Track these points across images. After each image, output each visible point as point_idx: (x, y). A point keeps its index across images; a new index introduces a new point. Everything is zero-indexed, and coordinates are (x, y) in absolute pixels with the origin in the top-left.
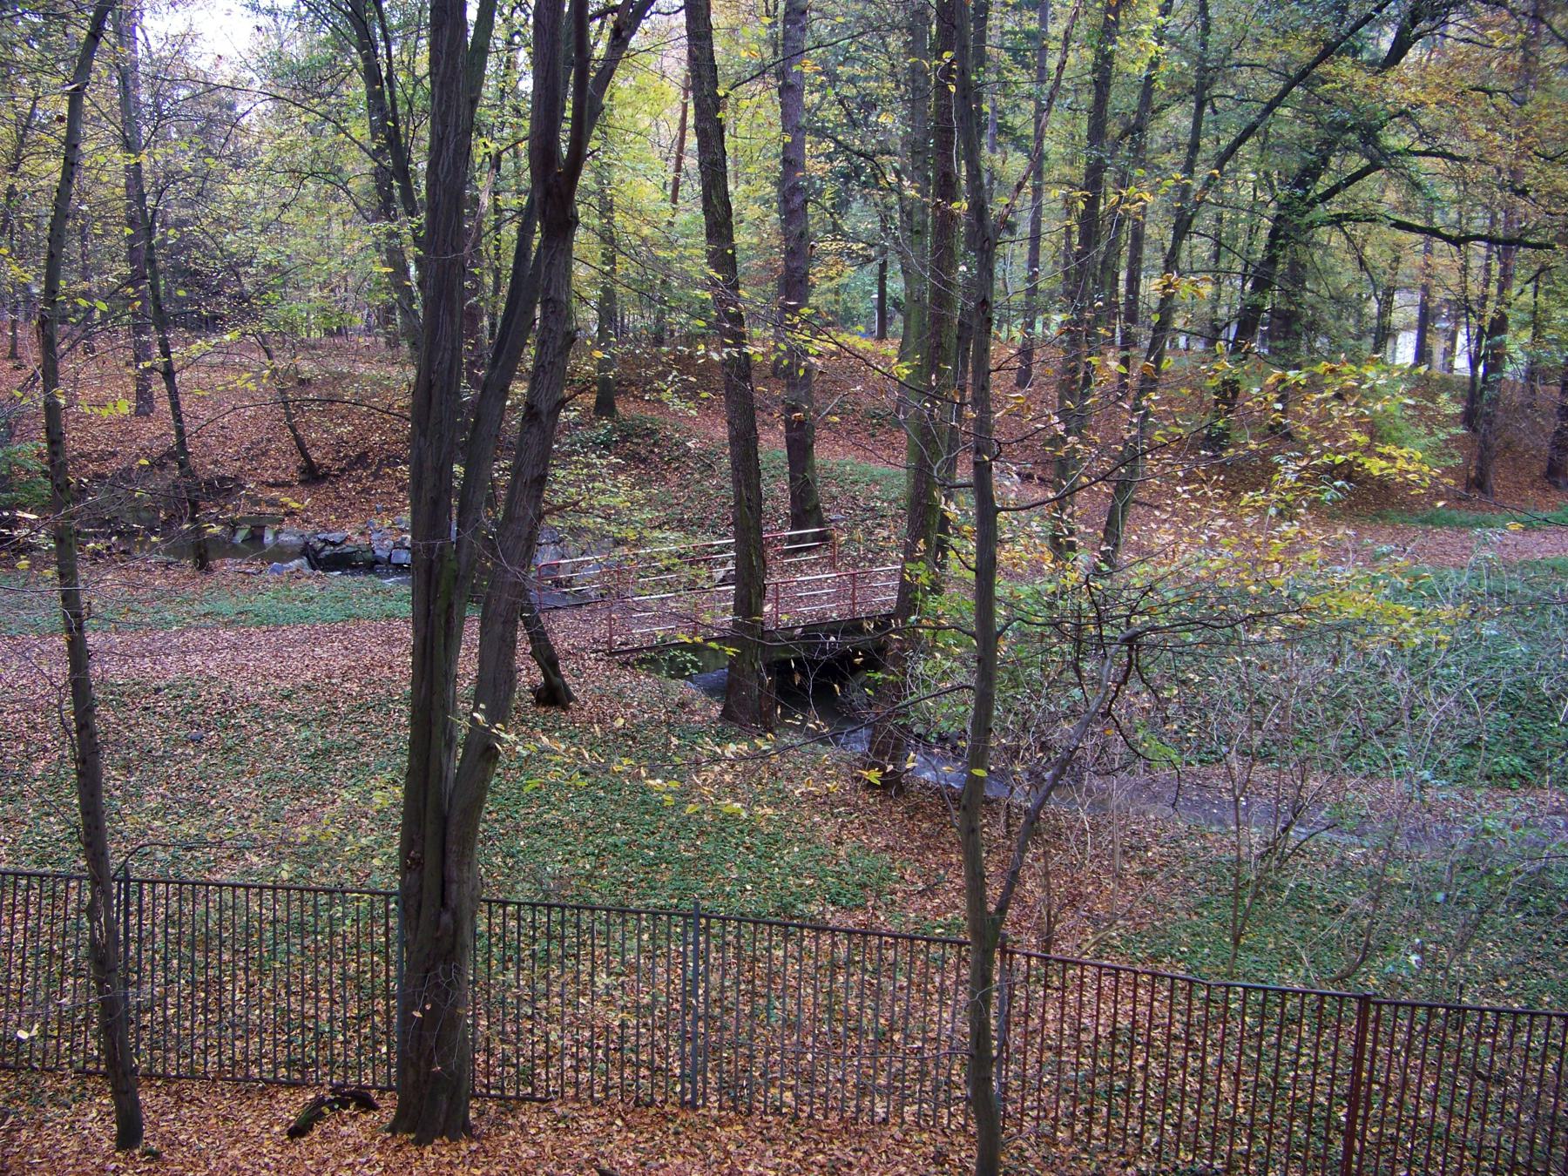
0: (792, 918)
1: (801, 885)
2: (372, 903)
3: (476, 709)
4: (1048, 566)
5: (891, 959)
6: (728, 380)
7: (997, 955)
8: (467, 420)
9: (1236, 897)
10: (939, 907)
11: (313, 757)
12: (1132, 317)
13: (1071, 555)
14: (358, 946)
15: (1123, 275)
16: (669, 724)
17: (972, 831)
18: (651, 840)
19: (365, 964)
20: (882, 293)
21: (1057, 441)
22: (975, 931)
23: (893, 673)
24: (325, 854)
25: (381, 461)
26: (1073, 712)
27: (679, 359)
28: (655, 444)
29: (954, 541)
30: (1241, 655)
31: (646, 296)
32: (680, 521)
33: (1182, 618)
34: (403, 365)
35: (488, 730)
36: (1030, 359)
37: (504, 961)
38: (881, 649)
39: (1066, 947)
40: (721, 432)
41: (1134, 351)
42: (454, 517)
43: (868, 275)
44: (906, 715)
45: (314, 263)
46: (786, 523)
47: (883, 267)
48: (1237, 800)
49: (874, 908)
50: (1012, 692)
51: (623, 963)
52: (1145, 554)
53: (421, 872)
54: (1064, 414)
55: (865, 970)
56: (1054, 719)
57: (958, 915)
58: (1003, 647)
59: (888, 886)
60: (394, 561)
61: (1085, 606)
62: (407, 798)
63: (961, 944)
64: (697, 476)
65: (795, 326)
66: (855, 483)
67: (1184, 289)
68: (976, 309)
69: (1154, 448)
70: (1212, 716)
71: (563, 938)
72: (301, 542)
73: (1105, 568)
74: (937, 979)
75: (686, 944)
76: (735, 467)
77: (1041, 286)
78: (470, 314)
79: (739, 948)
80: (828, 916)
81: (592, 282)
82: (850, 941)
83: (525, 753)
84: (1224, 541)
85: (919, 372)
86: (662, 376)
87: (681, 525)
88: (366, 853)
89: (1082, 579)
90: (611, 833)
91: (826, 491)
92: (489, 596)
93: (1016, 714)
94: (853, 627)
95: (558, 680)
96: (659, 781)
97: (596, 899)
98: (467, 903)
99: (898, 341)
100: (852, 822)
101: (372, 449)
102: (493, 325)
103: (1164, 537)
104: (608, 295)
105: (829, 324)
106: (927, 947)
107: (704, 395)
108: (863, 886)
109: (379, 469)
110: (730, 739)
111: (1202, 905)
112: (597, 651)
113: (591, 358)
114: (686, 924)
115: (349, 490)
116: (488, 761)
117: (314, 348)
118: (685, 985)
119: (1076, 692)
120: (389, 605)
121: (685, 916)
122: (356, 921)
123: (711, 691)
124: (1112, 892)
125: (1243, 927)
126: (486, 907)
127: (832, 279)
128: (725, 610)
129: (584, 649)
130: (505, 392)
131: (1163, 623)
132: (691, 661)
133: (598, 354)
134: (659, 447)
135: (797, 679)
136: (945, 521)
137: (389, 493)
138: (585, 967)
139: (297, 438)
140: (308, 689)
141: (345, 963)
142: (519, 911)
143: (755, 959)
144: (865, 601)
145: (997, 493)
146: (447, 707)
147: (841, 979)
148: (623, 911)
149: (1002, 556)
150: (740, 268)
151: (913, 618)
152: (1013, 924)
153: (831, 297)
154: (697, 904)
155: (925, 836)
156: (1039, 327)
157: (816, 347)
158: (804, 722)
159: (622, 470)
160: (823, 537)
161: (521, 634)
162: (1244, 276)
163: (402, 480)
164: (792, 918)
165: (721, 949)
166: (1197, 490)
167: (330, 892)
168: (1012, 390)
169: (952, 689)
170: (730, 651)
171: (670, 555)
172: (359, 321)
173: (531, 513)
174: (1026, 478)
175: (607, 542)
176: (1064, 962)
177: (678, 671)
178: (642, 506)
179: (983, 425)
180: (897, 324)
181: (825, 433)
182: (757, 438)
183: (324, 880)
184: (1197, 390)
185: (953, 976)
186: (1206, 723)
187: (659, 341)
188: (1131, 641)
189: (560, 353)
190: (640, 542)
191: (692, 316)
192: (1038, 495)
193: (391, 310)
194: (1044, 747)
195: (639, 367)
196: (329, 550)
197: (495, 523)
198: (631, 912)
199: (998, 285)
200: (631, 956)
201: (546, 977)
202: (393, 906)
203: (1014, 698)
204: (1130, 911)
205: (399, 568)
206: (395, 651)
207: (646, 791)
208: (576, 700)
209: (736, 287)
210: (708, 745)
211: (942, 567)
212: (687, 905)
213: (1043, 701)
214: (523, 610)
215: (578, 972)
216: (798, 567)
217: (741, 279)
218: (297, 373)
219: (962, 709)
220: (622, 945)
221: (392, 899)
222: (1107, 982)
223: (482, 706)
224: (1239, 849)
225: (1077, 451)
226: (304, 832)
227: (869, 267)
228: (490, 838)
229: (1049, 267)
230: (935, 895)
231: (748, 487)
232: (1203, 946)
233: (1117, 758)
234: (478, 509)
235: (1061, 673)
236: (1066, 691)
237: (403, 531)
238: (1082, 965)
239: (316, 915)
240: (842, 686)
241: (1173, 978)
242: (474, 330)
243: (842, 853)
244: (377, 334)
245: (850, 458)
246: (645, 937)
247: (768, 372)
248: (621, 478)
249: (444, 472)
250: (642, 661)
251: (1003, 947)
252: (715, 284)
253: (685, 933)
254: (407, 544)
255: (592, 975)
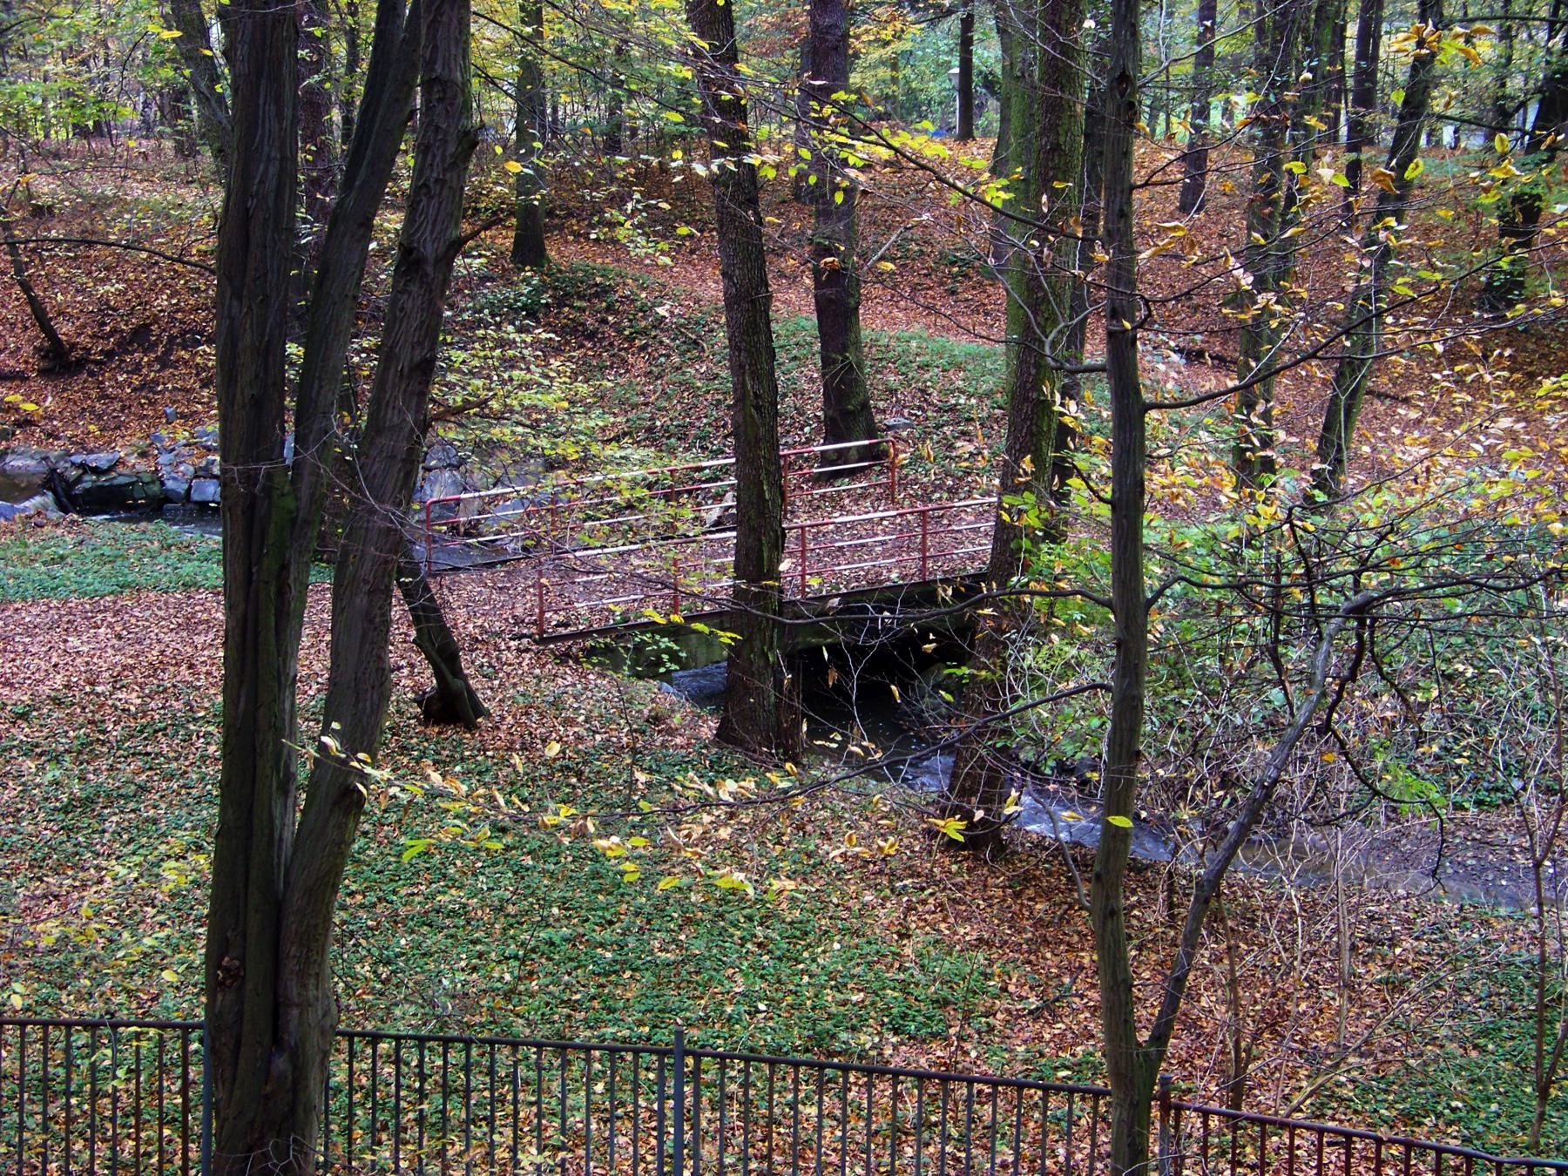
0: (831, 1054)
1: (844, 1003)
2: (161, 1043)
3: (326, 730)
4: (1227, 495)
5: (987, 1119)
6: (722, 209)
7: (1155, 1113)
8: (309, 272)
9: (1541, 1022)
10: (1063, 1035)
11: (66, 810)
12: (1365, 97)
13: (1267, 479)
14: (137, 1113)
15: (1352, 30)
16: (634, 751)
17: (1109, 913)
18: (607, 935)
19: (149, 1142)
20: (966, 64)
21: (1240, 299)
22: (1117, 1074)
23: (987, 668)
24: (85, 964)
25: (171, 339)
26: (1271, 724)
27: (643, 176)
28: (610, 309)
29: (1081, 461)
30: (1542, 632)
31: (591, 75)
32: (650, 430)
33: (1444, 575)
34: (204, 186)
35: (345, 762)
36: (1199, 167)
37: (374, 1130)
38: (968, 628)
39: (1266, 1100)
40: (713, 289)
41: (1366, 154)
42: (290, 427)
43: (945, 36)
44: (1007, 733)
45: (51, 17)
46: (817, 431)
47: (968, 24)
48: (1538, 865)
49: (960, 1038)
50: (1174, 694)
51: (563, 1130)
52: (1381, 475)
53: (240, 989)
54: (1251, 258)
55: (946, 1138)
56: (1242, 738)
57: (1093, 1049)
58: (1157, 627)
59: (982, 1003)
60: (195, 497)
61: (1288, 556)
62: (217, 873)
63: (1098, 1094)
64: (676, 359)
65: (825, 121)
66: (924, 367)
67: (1450, 50)
68: (1111, 89)
69: (1398, 305)
70: (1495, 731)
71: (467, 1091)
72: (43, 468)
73: (1321, 497)
74: (1061, 1151)
75: (662, 1099)
76: (734, 345)
77: (1220, 49)
78: (311, 103)
79: (747, 1103)
80: (888, 1051)
81: (505, 52)
82: (920, 1088)
83: (404, 797)
84: (1511, 453)
85: (1026, 192)
86: (618, 201)
87: (652, 437)
88: (152, 962)
89: (1282, 516)
90: (545, 923)
91: (878, 381)
92: (345, 553)
93: (1181, 730)
94: (922, 593)
95: (459, 683)
96: (615, 839)
97: (520, 1028)
98: (315, 1038)
99: (991, 142)
100: (924, 902)
101: (156, 319)
102: (347, 120)
103: (1412, 450)
104: (530, 72)
105: (879, 117)
106: (1045, 1099)
107: (683, 230)
108: (943, 1003)
109: (168, 352)
110: (731, 773)
111: (1485, 1033)
112: (520, 637)
113: (506, 173)
114: (662, 1066)
115: (120, 386)
116: (347, 813)
117: (57, 156)
118: (661, 1164)
119: (1276, 695)
120: (188, 568)
121: (662, 1054)
122: (134, 1072)
123: (701, 698)
124: (1339, 1012)
125: (1553, 1070)
126: (345, 1045)
127: (887, 43)
128: (721, 569)
129: (499, 634)
130: (366, 228)
131: (1413, 582)
132: (668, 650)
133: (514, 167)
134: (616, 313)
135: (833, 676)
136: (1065, 431)
137: (184, 390)
138: (504, 1137)
139: (32, 301)
140: (57, 702)
141: (115, 1141)
142: (397, 1050)
143: (772, 1121)
144: (942, 554)
145: (1144, 380)
146: (281, 725)
147: (909, 1151)
148: (563, 1047)
149: (1155, 482)
150: (741, 28)
151: (1015, 579)
152: (1181, 1063)
153: (884, 73)
154: (680, 1035)
155: (1039, 923)
156: (1216, 117)
157: (861, 152)
158: (843, 745)
159: (558, 351)
160: (874, 454)
161: (398, 610)
162: (1552, 24)
163: (205, 368)
164: (831, 1054)
165: (718, 1106)
166: (1468, 373)
167: (92, 1026)
168: (1172, 217)
169: (1079, 690)
170: (726, 637)
171: (634, 483)
172: (129, 114)
173: (410, 418)
174: (1193, 356)
175: (533, 465)
176: (1262, 1122)
177: (648, 667)
178: (589, 407)
179: (1122, 273)
180: (990, 115)
181: (877, 290)
182: (769, 298)
183: (83, 1007)
184: (1473, 213)
185: (1086, 1145)
186: (1485, 740)
187: (613, 146)
188: (1362, 612)
189: (453, 165)
190: (586, 463)
191: (664, 105)
192: (1210, 384)
193: (180, 95)
194: (1226, 782)
195: (583, 186)
196: (89, 481)
197: (355, 434)
198: (576, 1047)
199: (1148, 50)
200: (576, 1119)
201: (441, 1153)
202: (195, 1046)
203: (1177, 703)
204: (1366, 1042)
205: (201, 512)
206: (199, 640)
207: (597, 857)
208: (488, 715)
209: (732, 57)
210: (694, 783)
211: (1061, 497)
212: (664, 1037)
213: (1223, 709)
214: (401, 573)
215: (492, 1144)
216: (836, 502)
217: (741, 46)
218: (30, 197)
219: (1095, 722)
220: (562, 1102)
221: (194, 1035)
222: (1332, 1155)
223: (335, 726)
224: (1543, 944)
225: (1273, 315)
226: (50, 931)
227: (945, 25)
228: (352, 934)
229: (1233, 18)
230: (1057, 1017)
231: (755, 375)
232: (1489, 1100)
233: (1343, 798)
234: (326, 415)
235: (1252, 664)
236: (1260, 692)
237: (209, 449)
238: (1292, 1128)
239: (69, 1065)
240: (904, 689)
241: (1440, 1151)
242: (316, 129)
243: (908, 951)
244: (161, 135)
245: (916, 328)
246: (599, 1087)
247: (787, 192)
248: (555, 363)
249: (272, 356)
250: (591, 652)
251: (1164, 1097)
252: (698, 54)
253: (661, 1081)
254: (216, 470)
255: (513, 1150)
